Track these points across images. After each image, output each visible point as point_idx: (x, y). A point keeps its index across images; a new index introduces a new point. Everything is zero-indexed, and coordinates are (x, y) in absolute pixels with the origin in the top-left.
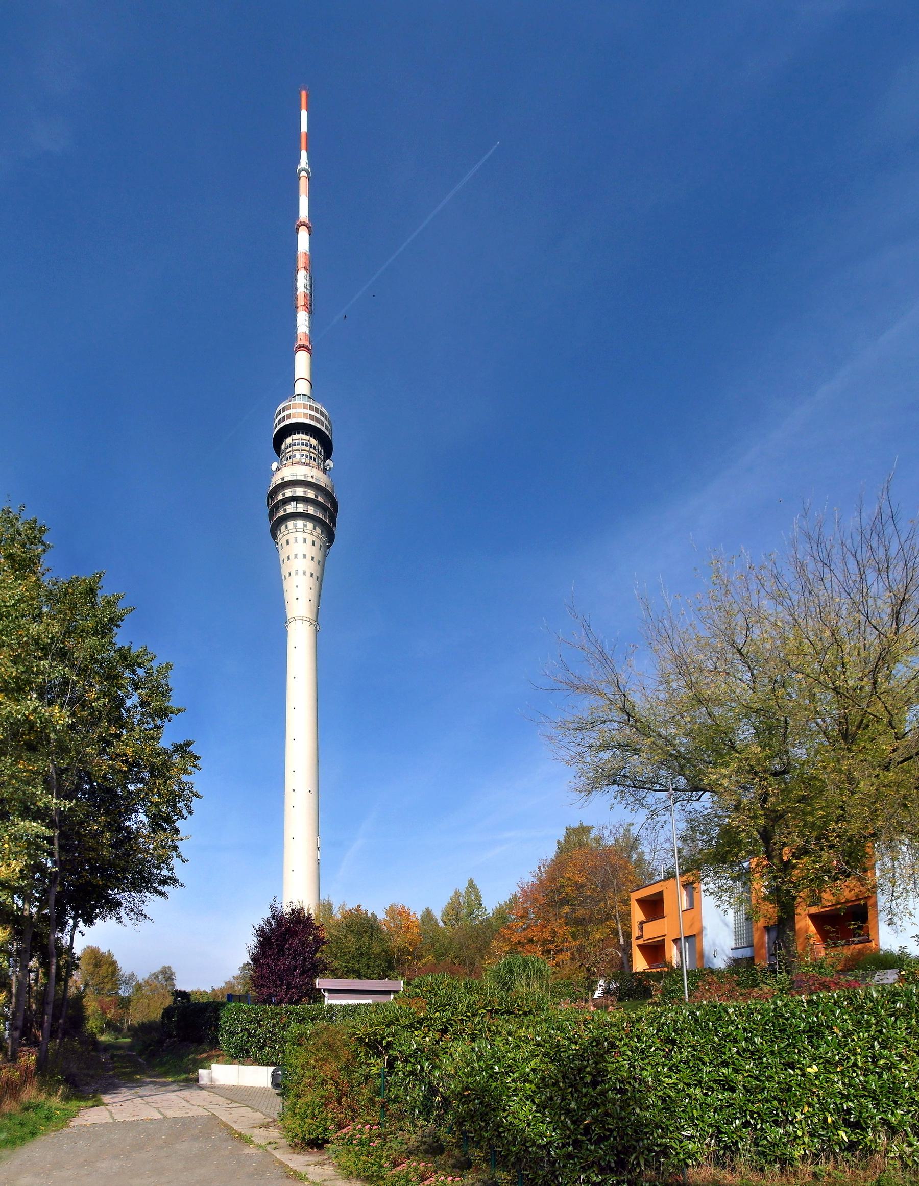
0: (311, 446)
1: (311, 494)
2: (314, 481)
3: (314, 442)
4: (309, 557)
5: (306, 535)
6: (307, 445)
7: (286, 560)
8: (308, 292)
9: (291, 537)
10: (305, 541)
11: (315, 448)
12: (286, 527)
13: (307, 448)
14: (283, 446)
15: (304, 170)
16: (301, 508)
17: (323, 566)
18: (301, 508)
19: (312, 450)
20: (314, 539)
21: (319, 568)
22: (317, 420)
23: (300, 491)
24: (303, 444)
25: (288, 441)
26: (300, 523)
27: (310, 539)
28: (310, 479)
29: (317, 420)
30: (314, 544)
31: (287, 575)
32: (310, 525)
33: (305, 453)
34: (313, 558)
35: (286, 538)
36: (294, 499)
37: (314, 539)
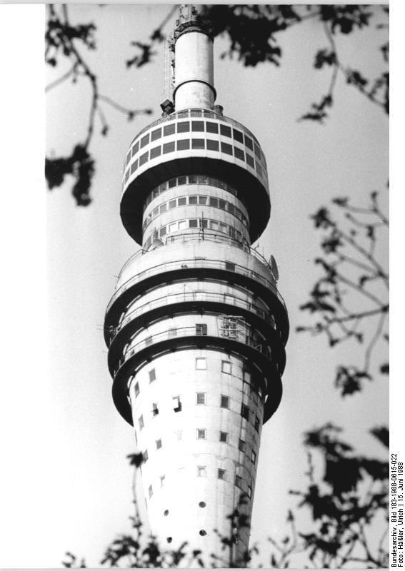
7: (189, 402)
16: (185, 325)
18: (185, 325)
26: (186, 357)
29: (227, 149)
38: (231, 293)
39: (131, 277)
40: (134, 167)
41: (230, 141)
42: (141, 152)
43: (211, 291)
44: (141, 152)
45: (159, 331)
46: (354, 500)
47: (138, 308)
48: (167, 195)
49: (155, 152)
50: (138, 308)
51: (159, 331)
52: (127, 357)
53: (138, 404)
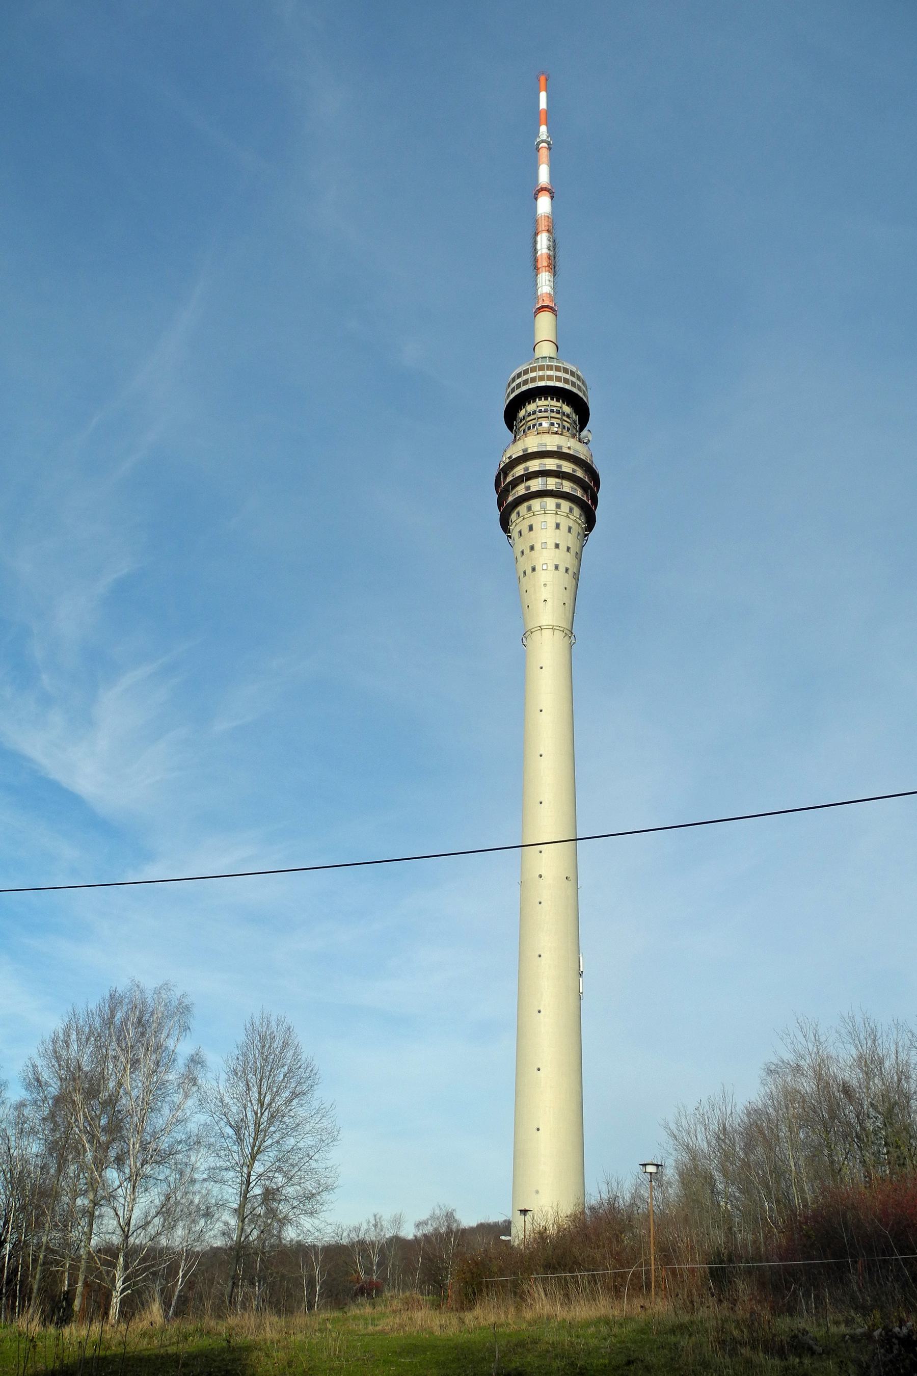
0: (564, 414)
1: (567, 467)
2: (571, 452)
3: (567, 409)
4: (563, 547)
5: (560, 519)
6: (558, 412)
7: (527, 551)
8: (552, 253)
9: (534, 521)
10: (558, 526)
11: (568, 416)
12: (518, 513)
13: (559, 416)
14: (522, 413)
15: (543, 141)
16: (551, 483)
17: (576, 576)
18: (551, 483)
19: (565, 418)
20: (571, 524)
21: (576, 562)
22: (566, 381)
23: (551, 464)
24: (552, 411)
25: (531, 407)
26: (550, 502)
27: (565, 523)
28: (565, 450)
29: (566, 381)
30: (569, 531)
31: (529, 571)
32: (565, 505)
33: (555, 421)
34: (568, 549)
35: (527, 523)
36: (530, 476)
37: (571, 524)
38: (545, 499)
39: (516, 451)
40: (513, 390)
41: (568, 376)
42: (518, 381)
43: (567, 467)
44: (518, 381)
45: (536, 485)
46: (36, 1166)
47: (519, 471)
48: (541, 403)
49: (519, 386)
50: (519, 471)
51: (536, 485)
52: (510, 499)
53: (514, 530)
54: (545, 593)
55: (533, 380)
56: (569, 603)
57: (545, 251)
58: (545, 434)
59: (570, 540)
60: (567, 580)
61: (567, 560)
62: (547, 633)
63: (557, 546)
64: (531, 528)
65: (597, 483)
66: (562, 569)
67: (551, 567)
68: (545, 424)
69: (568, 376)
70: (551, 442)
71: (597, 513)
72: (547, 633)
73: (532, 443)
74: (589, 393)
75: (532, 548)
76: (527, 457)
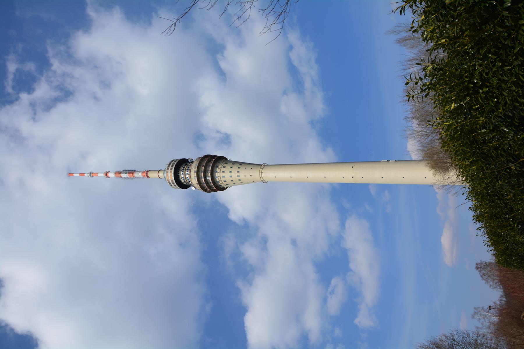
10: (223, 172)
14: (183, 181)
17: (241, 164)
33: (186, 173)
34: (231, 167)
41: (170, 168)
51: (209, 178)
54: (248, 175)
55: (172, 181)
56: (250, 167)
57: (127, 175)
58: (190, 175)
59: (228, 166)
60: (242, 167)
61: (235, 167)
62: (263, 175)
63: (231, 172)
64: (225, 181)
65: (206, 156)
66: (239, 170)
67: (238, 174)
68: (187, 176)
69: (170, 168)
70: (194, 175)
71: (213, 155)
72: (263, 175)
73: (194, 181)
74: (175, 158)
75: (232, 181)
76: (200, 183)
